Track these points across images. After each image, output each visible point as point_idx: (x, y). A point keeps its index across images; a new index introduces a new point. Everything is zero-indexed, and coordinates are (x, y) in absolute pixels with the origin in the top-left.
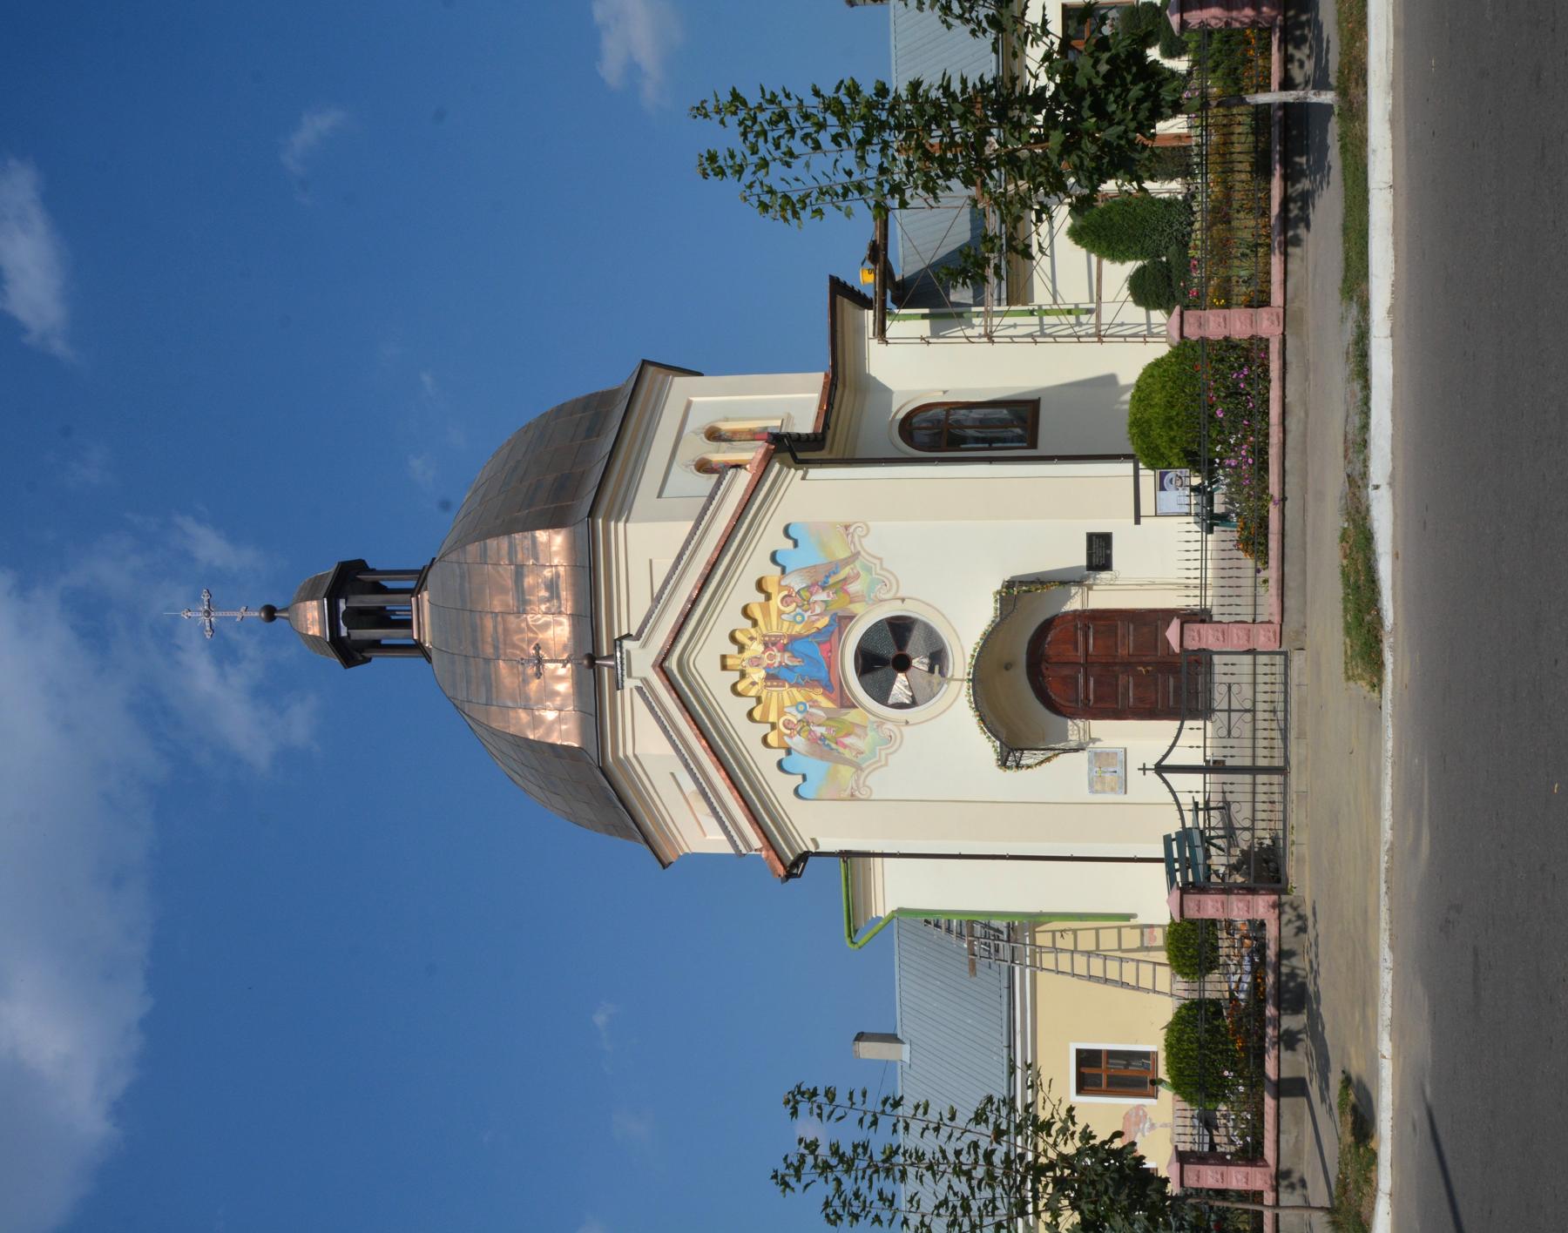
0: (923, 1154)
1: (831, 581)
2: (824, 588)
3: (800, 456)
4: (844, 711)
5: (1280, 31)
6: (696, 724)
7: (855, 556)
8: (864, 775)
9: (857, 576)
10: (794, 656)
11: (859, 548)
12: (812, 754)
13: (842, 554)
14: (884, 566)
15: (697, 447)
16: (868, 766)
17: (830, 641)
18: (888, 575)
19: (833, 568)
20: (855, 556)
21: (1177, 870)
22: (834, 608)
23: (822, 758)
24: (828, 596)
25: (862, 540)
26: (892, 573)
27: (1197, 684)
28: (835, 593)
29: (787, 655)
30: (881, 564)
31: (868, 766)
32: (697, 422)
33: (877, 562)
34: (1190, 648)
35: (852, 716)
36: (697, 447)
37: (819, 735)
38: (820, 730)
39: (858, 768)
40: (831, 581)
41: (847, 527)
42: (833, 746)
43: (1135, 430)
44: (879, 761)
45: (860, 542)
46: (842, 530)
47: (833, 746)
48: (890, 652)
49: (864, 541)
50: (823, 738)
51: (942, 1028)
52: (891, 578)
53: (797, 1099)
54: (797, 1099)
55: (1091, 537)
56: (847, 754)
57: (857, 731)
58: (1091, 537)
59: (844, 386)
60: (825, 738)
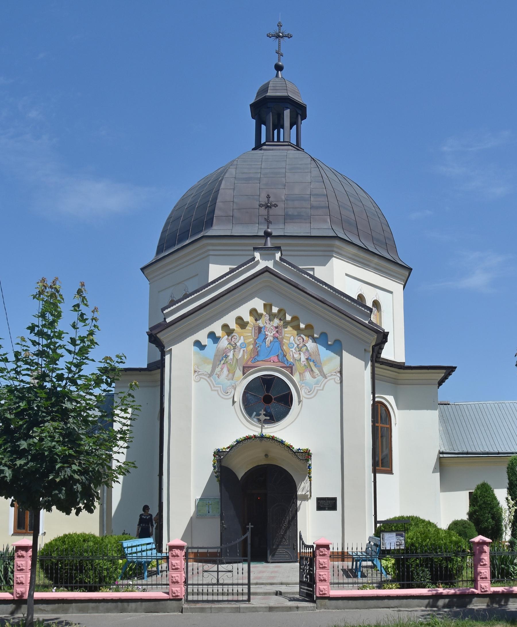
1: (311, 363)
2: (307, 359)
4: (241, 368)
7: (325, 377)
10: (271, 342)
11: (328, 378)
17: (280, 362)
20: (325, 377)
22: (297, 364)
24: (303, 362)
26: (315, 396)
28: (305, 365)
29: (272, 339)
35: (239, 373)
38: (231, 355)
39: (210, 375)
40: (311, 363)
42: (222, 362)
50: (226, 357)
56: (218, 370)
57: (231, 375)
60: (226, 358)
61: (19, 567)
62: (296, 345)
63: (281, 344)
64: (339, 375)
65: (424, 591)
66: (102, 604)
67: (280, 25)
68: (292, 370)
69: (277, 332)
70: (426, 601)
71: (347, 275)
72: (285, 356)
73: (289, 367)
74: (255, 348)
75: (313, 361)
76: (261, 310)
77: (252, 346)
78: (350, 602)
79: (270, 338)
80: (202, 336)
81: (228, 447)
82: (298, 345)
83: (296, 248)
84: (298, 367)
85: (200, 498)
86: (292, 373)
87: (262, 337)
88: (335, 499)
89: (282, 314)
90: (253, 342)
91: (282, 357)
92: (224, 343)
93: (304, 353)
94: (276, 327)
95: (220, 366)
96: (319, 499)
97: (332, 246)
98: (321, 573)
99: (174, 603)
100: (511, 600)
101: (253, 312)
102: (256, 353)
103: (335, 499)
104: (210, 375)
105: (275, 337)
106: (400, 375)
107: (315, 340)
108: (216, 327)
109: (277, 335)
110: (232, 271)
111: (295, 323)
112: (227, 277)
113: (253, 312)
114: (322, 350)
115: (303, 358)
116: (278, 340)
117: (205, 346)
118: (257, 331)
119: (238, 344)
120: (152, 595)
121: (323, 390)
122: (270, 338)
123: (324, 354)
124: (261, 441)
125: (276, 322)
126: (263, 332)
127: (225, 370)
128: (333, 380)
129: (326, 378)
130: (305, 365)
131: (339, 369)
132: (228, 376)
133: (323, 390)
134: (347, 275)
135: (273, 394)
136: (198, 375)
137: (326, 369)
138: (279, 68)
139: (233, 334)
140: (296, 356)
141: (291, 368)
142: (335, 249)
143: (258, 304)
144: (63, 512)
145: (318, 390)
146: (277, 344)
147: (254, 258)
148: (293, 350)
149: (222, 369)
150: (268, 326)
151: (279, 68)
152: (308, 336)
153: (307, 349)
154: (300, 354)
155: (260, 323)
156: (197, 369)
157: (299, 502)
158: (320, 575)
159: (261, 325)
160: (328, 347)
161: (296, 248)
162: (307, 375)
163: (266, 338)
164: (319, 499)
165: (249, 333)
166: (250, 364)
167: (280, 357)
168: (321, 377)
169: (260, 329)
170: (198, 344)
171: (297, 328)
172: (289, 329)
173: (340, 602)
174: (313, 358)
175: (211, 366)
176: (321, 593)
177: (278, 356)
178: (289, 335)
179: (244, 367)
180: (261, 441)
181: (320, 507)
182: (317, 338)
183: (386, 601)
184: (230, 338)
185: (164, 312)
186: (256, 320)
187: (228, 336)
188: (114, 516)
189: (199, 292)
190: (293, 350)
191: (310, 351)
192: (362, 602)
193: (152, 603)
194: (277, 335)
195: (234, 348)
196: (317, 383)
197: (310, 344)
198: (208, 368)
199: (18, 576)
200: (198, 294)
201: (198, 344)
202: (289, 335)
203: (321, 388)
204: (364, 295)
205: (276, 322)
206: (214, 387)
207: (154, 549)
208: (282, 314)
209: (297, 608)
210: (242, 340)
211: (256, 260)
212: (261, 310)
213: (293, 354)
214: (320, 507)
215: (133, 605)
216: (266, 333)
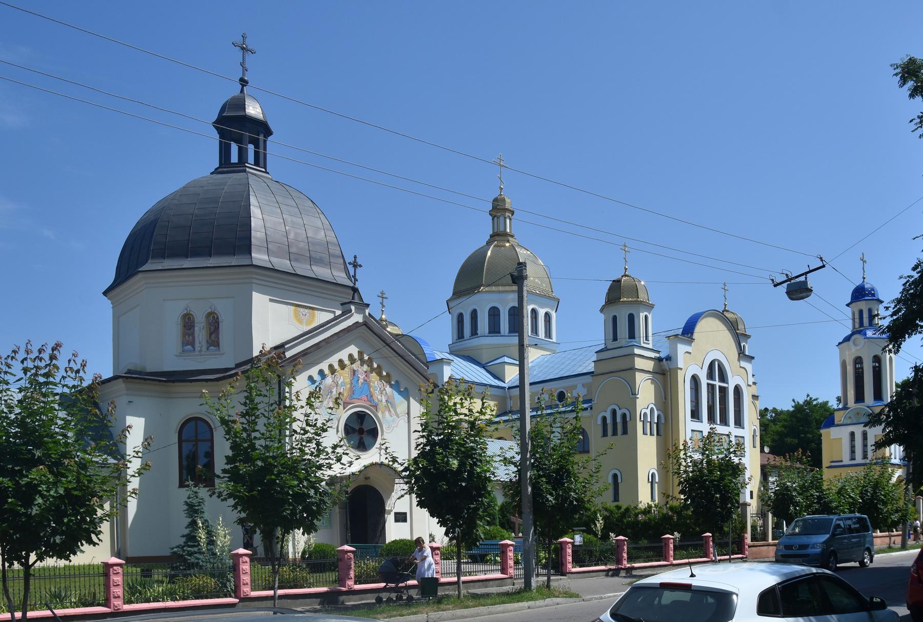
1: (389, 404)
2: (386, 401)
3: (794, 297)
5: (558, 539)
10: (362, 383)
14: (395, 428)
17: (368, 401)
18: (392, 429)
21: (24, 614)
22: (380, 404)
25: (403, 420)
26: (392, 431)
29: (362, 381)
33: (396, 425)
38: (334, 390)
40: (389, 404)
42: (329, 397)
45: (402, 419)
48: (357, 427)
50: (331, 392)
52: (390, 431)
53: (382, 296)
54: (382, 296)
55: (627, 434)
58: (627, 434)
60: (331, 393)
62: (379, 389)
64: (407, 416)
65: (603, 567)
66: (477, 583)
69: (366, 375)
70: (605, 573)
72: (372, 396)
74: (351, 388)
75: (391, 404)
76: (356, 356)
79: (361, 381)
87: (356, 379)
88: (405, 514)
89: (370, 360)
90: (350, 382)
91: (370, 397)
93: (384, 396)
94: (366, 372)
95: (327, 400)
96: (396, 514)
98: (244, 578)
99: (509, 580)
100: (633, 571)
101: (351, 356)
103: (405, 514)
105: (365, 380)
107: (391, 386)
109: (366, 378)
110: (336, 318)
111: (379, 371)
113: (351, 356)
114: (396, 394)
115: (384, 401)
116: (366, 382)
118: (352, 373)
121: (396, 427)
122: (361, 381)
123: (398, 399)
124: (380, 467)
125: (365, 367)
128: (403, 420)
131: (406, 412)
135: (357, 427)
137: (399, 411)
139: (336, 373)
140: (379, 397)
141: (376, 407)
143: (353, 350)
144: (432, 515)
145: (394, 427)
146: (366, 385)
148: (377, 392)
150: (360, 370)
152: (387, 382)
153: (386, 393)
155: (355, 366)
158: (244, 580)
159: (355, 369)
160: (400, 393)
162: (387, 413)
164: (396, 514)
166: (348, 400)
167: (369, 397)
168: (395, 416)
169: (354, 371)
171: (379, 374)
172: (374, 374)
173: (575, 575)
176: (245, 594)
178: (374, 380)
180: (380, 467)
181: (397, 520)
182: (393, 384)
183: (591, 573)
184: (333, 376)
186: (352, 364)
187: (332, 374)
188: (130, 527)
189: (312, 333)
190: (377, 392)
191: (388, 395)
193: (499, 581)
194: (366, 378)
195: (337, 386)
196: (393, 421)
197: (388, 389)
200: (311, 334)
202: (374, 380)
205: (365, 367)
208: (370, 360)
209: (561, 579)
210: (342, 380)
212: (356, 356)
213: (377, 396)
214: (397, 520)
215: (491, 583)
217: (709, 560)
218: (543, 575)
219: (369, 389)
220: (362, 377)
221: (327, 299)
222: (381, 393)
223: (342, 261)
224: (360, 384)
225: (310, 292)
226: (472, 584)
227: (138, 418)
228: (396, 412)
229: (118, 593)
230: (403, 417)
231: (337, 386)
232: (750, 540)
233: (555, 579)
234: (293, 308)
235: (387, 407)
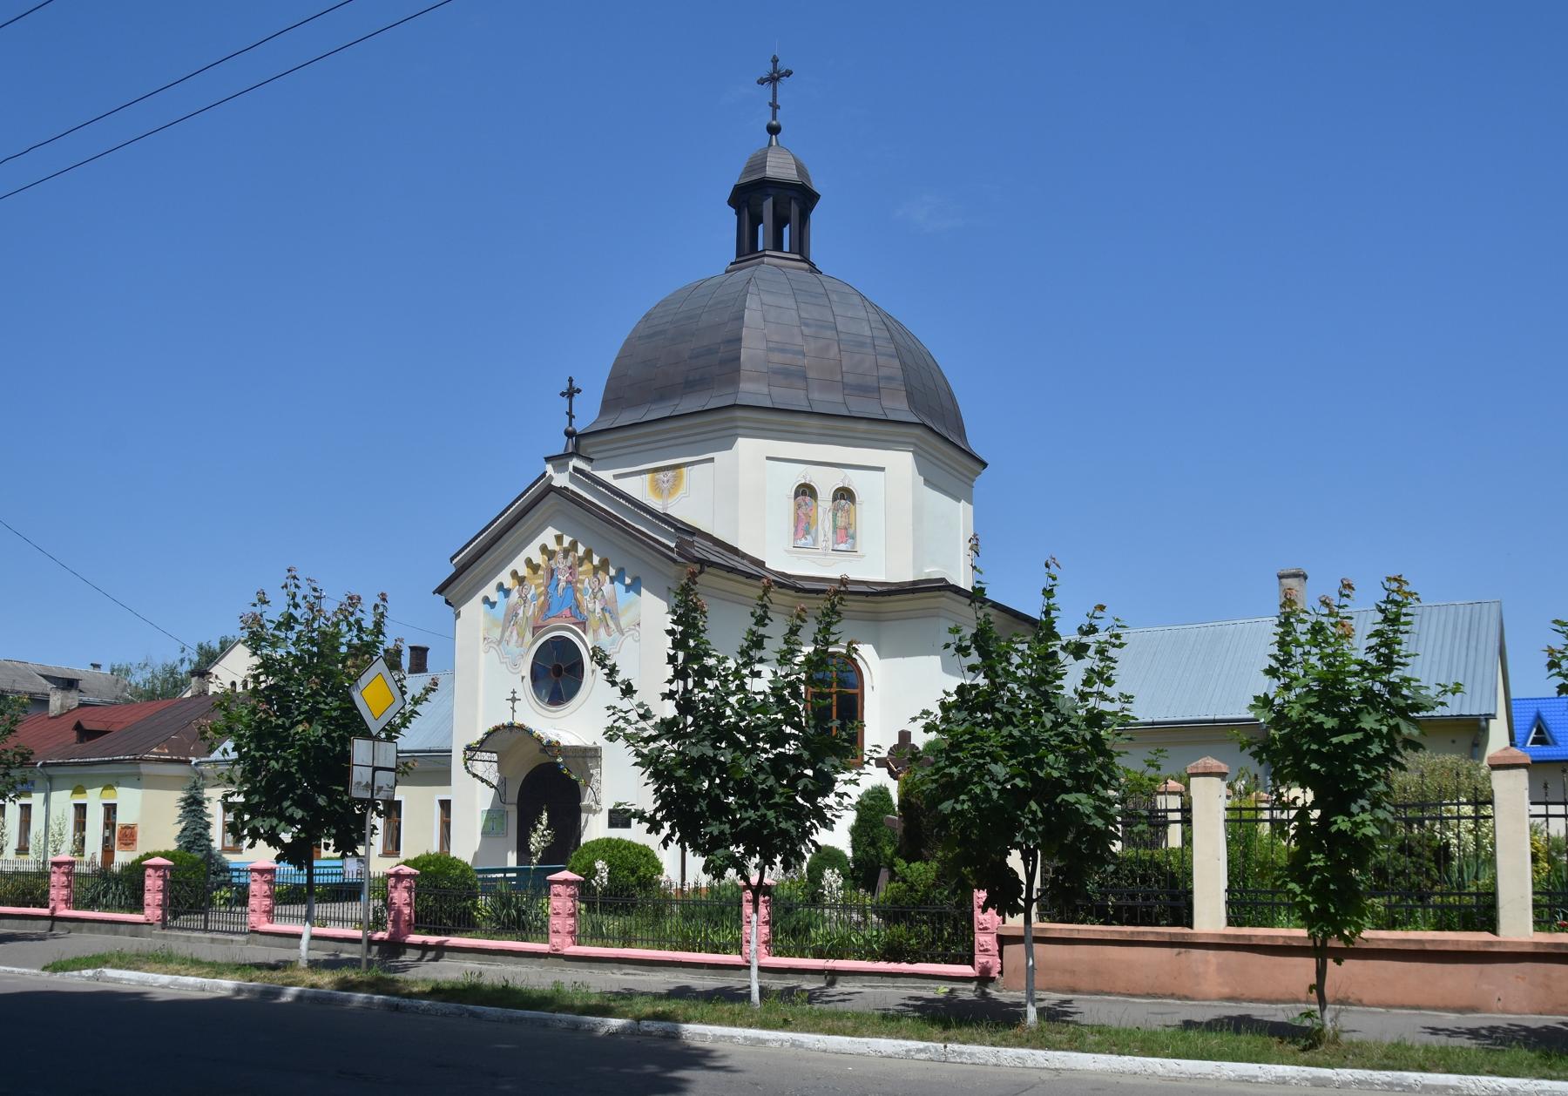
0: (296, 609)
1: (607, 615)
2: (602, 609)
4: (531, 629)
6: (501, 537)
7: (622, 633)
8: (495, 646)
9: (609, 635)
11: (626, 635)
12: (508, 608)
13: (623, 622)
15: (826, 483)
16: (500, 650)
19: (615, 618)
20: (622, 633)
22: (591, 617)
23: (505, 615)
24: (598, 613)
27: (701, 1021)
28: (600, 619)
29: (564, 584)
30: (616, 653)
31: (500, 650)
32: (856, 481)
34: (88, 728)
35: (528, 637)
36: (826, 483)
37: (518, 612)
38: (521, 612)
39: (500, 642)
40: (607, 615)
41: (639, 624)
42: (512, 623)
43: (1404, 928)
44: (503, 658)
45: (629, 635)
46: (637, 621)
47: (512, 623)
49: (630, 639)
50: (516, 615)
51: (34, 721)
52: (513, 671)
56: (507, 634)
57: (520, 640)
59: (800, 597)
60: (516, 617)
61: (982, 924)
62: (590, 590)
63: (575, 590)
67: (775, 61)
68: (585, 627)
69: (571, 574)
71: (768, 458)
72: (578, 607)
73: (582, 623)
75: (610, 613)
77: (543, 598)
78: (277, 938)
79: (562, 584)
80: (490, 590)
81: (478, 743)
82: (593, 590)
83: (643, 441)
84: (592, 621)
85: (489, 810)
86: (584, 632)
87: (554, 582)
92: (514, 596)
95: (510, 629)
97: (733, 420)
102: (546, 608)
104: (500, 642)
105: (568, 582)
106: (879, 605)
108: (505, 577)
112: (517, 504)
115: (598, 610)
117: (496, 603)
119: (529, 596)
120: (632, 954)
122: (562, 584)
126: (555, 577)
127: (515, 633)
129: (498, 645)
130: (600, 619)
132: (517, 642)
133: (619, 652)
134: (768, 458)
136: (488, 643)
138: (774, 130)
142: (740, 424)
143: (548, 536)
147: (544, 474)
148: (587, 597)
149: (512, 633)
151: (774, 130)
153: (603, 595)
154: (595, 602)
156: (487, 636)
157: (584, 816)
161: (643, 441)
162: (602, 631)
163: (558, 585)
165: (542, 576)
166: (540, 623)
169: (552, 571)
170: (486, 600)
173: (268, 938)
174: (609, 607)
175: (500, 629)
177: (570, 608)
179: (534, 628)
185: (454, 562)
190: (587, 597)
191: (606, 598)
192: (284, 940)
195: (525, 603)
198: (497, 633)
199: (555, 922)
201: (486, 600)
203: (617, 650)
204: (812, 484)
206: (503, 658)
207: (316, 875)
211: (547, 475)
215: (122, 927)
216: (559, 577)
217: (46, 912)
218: (222, 931)
219: (575, 595)
220: (563, 578)
221: (619, 455)
222: (595, 598)
223: (841, 346)
224: (560, 591)
225: (665, 444)
226: (97, 925)
227: (927, 657)
228: (618, 625)
229: (557, 926)
230: (633, 632)
231: (525, 603)
232: (1529, 917)
233: (221, 939)
234: (647, 477)
235: (603, 621)
